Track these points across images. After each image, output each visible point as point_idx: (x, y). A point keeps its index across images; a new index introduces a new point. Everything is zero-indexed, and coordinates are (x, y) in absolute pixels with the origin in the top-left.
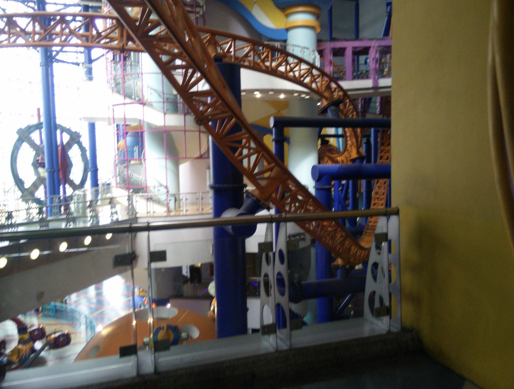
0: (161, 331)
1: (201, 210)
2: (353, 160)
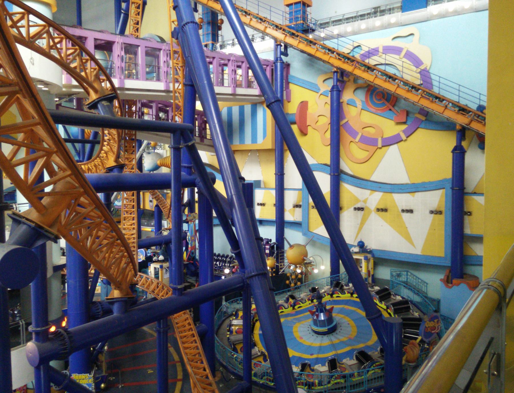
2: (110, 170)
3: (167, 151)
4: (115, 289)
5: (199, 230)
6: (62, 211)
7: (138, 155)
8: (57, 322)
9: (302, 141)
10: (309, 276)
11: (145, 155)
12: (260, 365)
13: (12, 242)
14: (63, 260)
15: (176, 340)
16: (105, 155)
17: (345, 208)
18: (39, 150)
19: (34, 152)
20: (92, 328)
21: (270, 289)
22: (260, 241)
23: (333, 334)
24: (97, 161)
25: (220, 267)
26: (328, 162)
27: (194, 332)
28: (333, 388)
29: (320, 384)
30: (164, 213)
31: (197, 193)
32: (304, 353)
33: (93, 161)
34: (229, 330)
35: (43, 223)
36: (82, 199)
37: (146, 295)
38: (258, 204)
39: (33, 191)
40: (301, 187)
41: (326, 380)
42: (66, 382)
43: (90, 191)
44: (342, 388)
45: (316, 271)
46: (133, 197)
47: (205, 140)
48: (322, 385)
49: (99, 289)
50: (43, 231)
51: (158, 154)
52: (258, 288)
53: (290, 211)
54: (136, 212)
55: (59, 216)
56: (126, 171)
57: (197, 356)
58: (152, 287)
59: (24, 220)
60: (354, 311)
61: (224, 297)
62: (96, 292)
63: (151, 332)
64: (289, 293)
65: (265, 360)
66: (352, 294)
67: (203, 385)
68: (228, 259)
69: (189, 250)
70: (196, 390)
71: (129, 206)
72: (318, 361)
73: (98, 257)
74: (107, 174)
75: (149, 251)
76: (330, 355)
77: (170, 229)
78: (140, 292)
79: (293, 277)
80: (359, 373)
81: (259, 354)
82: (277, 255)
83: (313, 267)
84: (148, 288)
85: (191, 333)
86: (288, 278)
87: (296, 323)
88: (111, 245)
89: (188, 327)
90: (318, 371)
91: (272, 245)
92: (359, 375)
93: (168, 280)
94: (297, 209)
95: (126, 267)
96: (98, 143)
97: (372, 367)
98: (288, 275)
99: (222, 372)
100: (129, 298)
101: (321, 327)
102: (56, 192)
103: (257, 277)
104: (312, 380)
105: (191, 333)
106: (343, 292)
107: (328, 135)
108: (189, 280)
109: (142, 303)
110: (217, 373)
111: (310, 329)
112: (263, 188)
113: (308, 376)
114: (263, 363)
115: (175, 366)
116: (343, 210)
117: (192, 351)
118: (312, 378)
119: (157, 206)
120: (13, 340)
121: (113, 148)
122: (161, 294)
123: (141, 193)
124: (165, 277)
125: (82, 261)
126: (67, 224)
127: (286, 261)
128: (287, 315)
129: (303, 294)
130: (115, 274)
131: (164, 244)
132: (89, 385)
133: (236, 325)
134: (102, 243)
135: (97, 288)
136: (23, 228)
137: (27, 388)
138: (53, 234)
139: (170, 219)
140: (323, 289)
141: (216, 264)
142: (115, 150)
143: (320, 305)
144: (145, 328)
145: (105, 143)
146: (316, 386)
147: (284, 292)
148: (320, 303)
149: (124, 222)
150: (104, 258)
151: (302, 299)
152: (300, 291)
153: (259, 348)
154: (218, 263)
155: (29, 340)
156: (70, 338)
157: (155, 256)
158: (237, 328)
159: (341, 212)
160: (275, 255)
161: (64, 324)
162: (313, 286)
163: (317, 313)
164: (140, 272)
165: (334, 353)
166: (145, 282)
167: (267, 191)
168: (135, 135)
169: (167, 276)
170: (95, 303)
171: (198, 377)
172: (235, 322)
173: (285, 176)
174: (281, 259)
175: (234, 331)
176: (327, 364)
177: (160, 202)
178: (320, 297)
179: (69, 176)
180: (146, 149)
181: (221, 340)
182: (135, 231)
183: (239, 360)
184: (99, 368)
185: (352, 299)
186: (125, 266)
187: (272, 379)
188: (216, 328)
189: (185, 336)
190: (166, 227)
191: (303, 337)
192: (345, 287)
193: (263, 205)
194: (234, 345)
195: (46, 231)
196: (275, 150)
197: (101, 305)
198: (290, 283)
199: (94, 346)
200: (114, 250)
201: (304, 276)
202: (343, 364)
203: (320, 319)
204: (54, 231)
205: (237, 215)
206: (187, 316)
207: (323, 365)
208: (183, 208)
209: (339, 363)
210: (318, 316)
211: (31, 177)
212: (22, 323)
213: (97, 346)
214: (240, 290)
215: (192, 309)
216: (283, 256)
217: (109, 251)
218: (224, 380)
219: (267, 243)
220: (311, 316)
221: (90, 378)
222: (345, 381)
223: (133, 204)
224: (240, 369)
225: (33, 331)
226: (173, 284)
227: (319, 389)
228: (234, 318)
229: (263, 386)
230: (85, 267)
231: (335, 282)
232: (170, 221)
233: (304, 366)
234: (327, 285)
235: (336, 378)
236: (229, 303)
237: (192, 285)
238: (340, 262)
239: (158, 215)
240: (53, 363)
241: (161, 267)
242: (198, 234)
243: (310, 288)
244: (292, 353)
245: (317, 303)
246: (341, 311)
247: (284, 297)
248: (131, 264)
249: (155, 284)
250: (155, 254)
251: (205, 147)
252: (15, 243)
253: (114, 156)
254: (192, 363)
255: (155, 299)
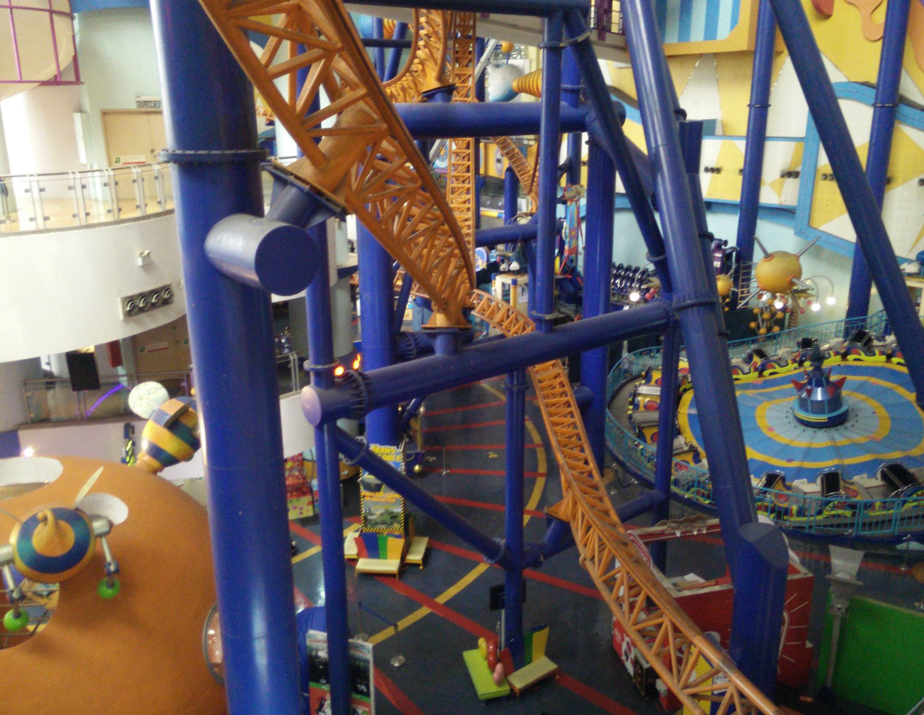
0: (40, 527)
1: (82, 215)
2: (429, 96)
3: (531, 61)
4: (438, 311)
5: (588, 218)
6: (352, 164)
7: (478, 70)
8: (347, 361)
9: (820, 31)
10: (800, 316)
11: (490, 69)
12: (687, 467)
13: (275, 216)
14: (352, 260)
15: (537, 410)
16: (420, 67)
17: (900, 180)
18: (311, 46)
19: (303, 51)
20: (404, 374)
21: (721, 334)
22: (707, 240)
23: (839, 427)
24: (406, 81)
25: (622, 289)
26: (873, 78)
27: (571, 399)
28: (828, 523)
29: (801, 513)
30: (522, 184)
31: (587, 142)
32: (775, 456)
33: (399, 79)
34: (632, 403)
35: (323, 186)
36: (385, 144)
37: (487, 329)
38: (707, 170)
39: (304, 124)
40: (803, 134)
41: (814, 508)
42: (362, 454)
43: (400, 130)
44: (845, 525)
45: (815, 307)
46: (468, 151)
47: (608, 34)
48: (804, 516)
49: (409, 313)
50: (323, 201)
51: (514, 67)
52: (696, 327)
53: (772, 184)
54: (472, 180)
55: (347, 174)
56: (456, 98)
57: (574, 438)
58: (498, 317)
59: (291, 178)
60: (891, 390)
61: (625, 343)
62: (405, 319)
63: (493, 391)
64: (754, 347)
65: (697, 459)
66: (889, 357)
67: (584, 487)
68: (638, 276)
69: (566, 254)
70: (571, 492)
71: (460, 168)
72: (799, 473)
73: (411, 252)
74: (425, 104)
75: (494, 253)
76: (828, 464)
77: (531, 214)
78: (476, 324)
79: (766, 315)
80: (885, 503)
81: (686, 448)
82: (737, 271)
83: (809, 299)
84: (492, 316)
85: (564, 399)
86: (754, 318)
87: (762, 402)
88: (432, 233)
89: (558, 389)
90: (798, 490)
91: (728, 252)
92: (884, 506)
93: (526, 306)
94: (790, 181)
95: (458, 274)
96: (408, 45)
97: (914, 496)
98: (756, 311)
99: (616, 471)
100: (461, 329)
101: (813, 412)
102: (343, 129)
103: (695, 309)
104: (785, 505)
105: (564, 399)
106: (870, 351)
107: (880, 16)
108: (562, 310)
109: (479, 342)
110: (606, 470)
111: (790, 416)
112: (720, 137)
113: (778, 496)
114: (692, 465)
115: (534, 453)
116: (892, 185)
117: (565, 429)
118: (786, 500)
119: (510, 170)
120: (282, 384)
121: (434, 51)
122: (513, 330)
123: (482, 145)
124: (520, 302)
125: (383, 257)
126: (360, 190)
127: (754, 285)
128: (746, 386)
129: (784, 350)
130: (438, 285)
131: (522, 242)
132: (398, 464)
133: (645, 395)
134: (417, 228)
135: (407, 311)
136: (290, 194)
137: (304, 460)
138: (338, 206)
139: (533, 194)
140: (827, 342)
141: (614, 283)
142: (438, 55)
143: (817, 373)
144: (485, 384)
145: (421, 43)
146: (792, 515)
147: (743, 343)
148: (818, 369)
149: (452, 196)
150: (420, 256)
151: (780, 359)
152: (777, 344)
153: (687, 438)
154: (618, 281)
155: (307, 383)
156: (367, 385)
157: (503, 262)
158: (648, 399)
159: (887, 187)
160: (732, 271)
161: (356, 365)
162: (805, 336)
163: (809, 387)
164: (478, 288)
165: (836, 462)
166: (486, 306)
167: (728, 142)
168: (474, 27)
169: (524, 299)
170: (404, 334)
171: (575, 473)
172: (643, 389)
173: (771, 112)
174: (743, 280)
175: (641, 405)
176: (819, 480)
177: (515, 161)
178: (818, 358)
179: (362, 98)
180: (492, 58)
181: (618, 417)
182: (470, 215)
183: (648, 455)
184: (412, 440)
185: (889, 365)
186: (455, 272)
187: (706, 493)
188: (608, 396)
189: (554, 405)
190: (524, 210)
191: (775, 428)
192: (876, 343)
193: (716, 170)
194: (641, 429)
195: (328, 200)
196: (755, 52)
197: (415, 340)
198: (759, 327)
199: (404, 403)
200: (437, 242)
201: (788, 315)
202: (852, 484)
203: (813, 398)
204: (340, 199)
205: (665, 188)
206: (558, 370)
207: (812, 480)
208: (559, 173)
209: (846, 482)
210: (810, 392)
211: (300, 103)
212: (293, 357)
213: (408, 405)
214: (657, 333)
215: (566, 359)
216: (749, 273)
217: (429, 244)
218: (618, 484)
219: (719, 247)
220: (795, 391)
221: (398, 454)
222: (854, 515)
223: (468, 163)
224: (649, 471)
225: (313, 369)
226: (538, 312)
227: (797, 522)
228: (643, 382)
229: (689, 502)
230: (389, 274)
231: (854, 332)
232: (533, 198)
233: (771, 479)
234: (836, 336)
235: (835, 507)
236: (635, 354)
237: (568, 319)
238: (874, 291)
239: (510, 187)
240: (342, 423)
241: (515, 282)
242: (583, 226)
243: (800, 340)
244: (752, 454)
245: (811, 369)
246: (860, 388)
247: (741, 353)
248: (464, 270)
249: (503, 310)
250: (504, 259)
251: (607, 50)
252: (281, 219)
253: (437, 69)
254: (565, 449)
255: (502, 336)
